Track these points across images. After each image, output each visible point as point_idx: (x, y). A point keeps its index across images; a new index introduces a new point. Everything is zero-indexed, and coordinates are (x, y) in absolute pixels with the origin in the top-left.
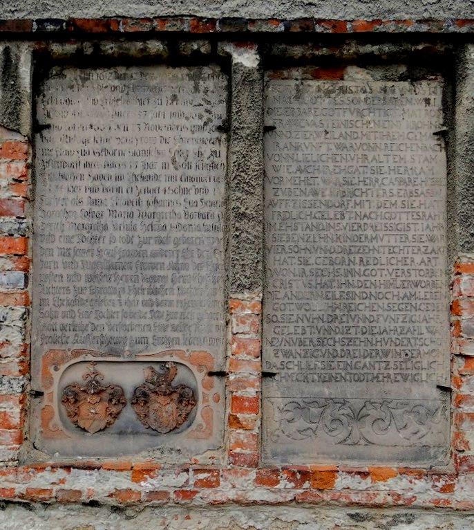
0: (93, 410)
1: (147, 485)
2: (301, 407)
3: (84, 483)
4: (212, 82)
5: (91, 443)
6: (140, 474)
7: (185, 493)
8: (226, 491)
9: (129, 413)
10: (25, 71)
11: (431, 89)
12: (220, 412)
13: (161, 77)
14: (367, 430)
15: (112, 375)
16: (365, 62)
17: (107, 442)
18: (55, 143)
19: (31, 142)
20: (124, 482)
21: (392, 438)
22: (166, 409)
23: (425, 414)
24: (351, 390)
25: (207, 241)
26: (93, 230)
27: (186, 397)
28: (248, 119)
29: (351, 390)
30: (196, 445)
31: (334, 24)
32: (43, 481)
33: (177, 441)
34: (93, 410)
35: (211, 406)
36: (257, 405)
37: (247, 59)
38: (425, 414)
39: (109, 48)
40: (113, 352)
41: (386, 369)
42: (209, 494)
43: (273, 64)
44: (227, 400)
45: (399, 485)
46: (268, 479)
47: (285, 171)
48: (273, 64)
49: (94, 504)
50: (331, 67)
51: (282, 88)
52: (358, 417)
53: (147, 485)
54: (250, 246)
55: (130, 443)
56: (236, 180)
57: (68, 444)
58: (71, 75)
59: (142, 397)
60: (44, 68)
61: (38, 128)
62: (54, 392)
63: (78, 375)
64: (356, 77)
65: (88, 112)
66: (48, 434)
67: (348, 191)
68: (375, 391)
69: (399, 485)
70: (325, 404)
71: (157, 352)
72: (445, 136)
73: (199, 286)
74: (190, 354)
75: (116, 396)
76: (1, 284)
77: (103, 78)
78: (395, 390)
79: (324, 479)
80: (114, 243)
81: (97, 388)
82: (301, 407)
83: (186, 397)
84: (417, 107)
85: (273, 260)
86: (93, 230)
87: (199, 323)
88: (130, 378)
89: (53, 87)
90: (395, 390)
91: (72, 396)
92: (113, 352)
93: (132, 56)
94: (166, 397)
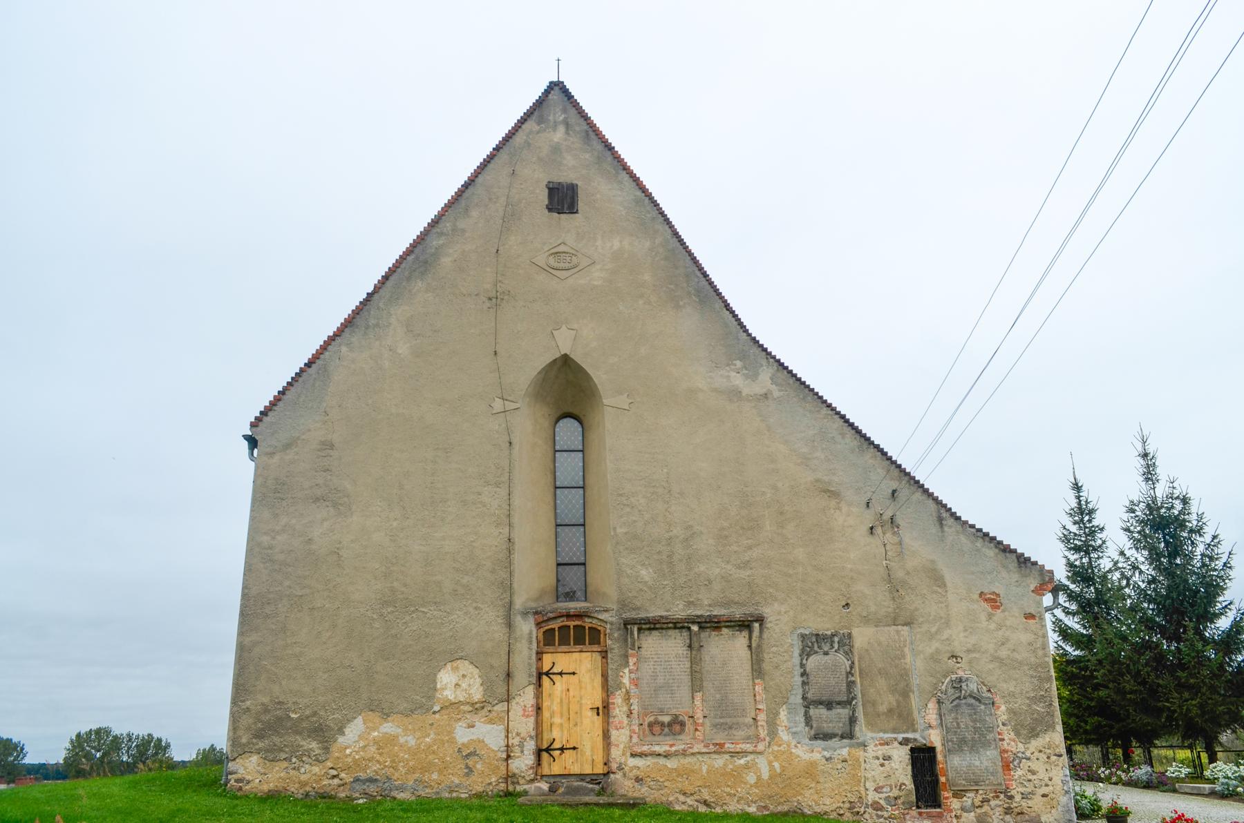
0: (657, 729)
1: (674, 749)
2: (715, 726)
3: (657, 749)
4: (685, 633)
5: (657, 738)
6: (671, 746)
9: (666, 730)
10: (636, 633)
11: (745, 633)
12: (692, 728)
13: (671, 632)
15: (661, 718)
17: (661, 738)
20: (667, 748)
21: (740, 734)
22: (677, 727)
23: (749, 726)
24: (728, 720)
25: (686, 679)
26: (654, 677)
27: (682, 724)
28: (696, 645)
29: (728, 720)
30: (685, 737)
31: (635, 798)
32: (645, 748)
33: (681, 737)
34: (657, 729)
35: (689, 726)
36: (702, 725)
38: (749, 726)
40: (662, 712)
44: (516, 447)
45: (743, 746)
46: (707, 746)
47: (706, 658)
51: (704, 635)
52: (731, 728)
53: (674, 749)
54: (696, 681)
56: (693, 662)
57: (650, 738)
59: (670, 725)
63: (652, 719)
65: (652, 644)
67: (724, 664)
68: (734, 720)
69: (743, 746)
71: (674, 711)
72: (750, 647)
73: (685, 691)
74: (682, 711)
75: (662, 724)
76: (1239, 756)
77: (655, 633)
78: (741, 720)
79: (722, 745)
80: (660, 680)
81: (656, 722)
82: (715, 726)
83: (682, 724)
84: (741, 640)
86: (654, 677)
87: (680, 701)
88: (666, 719)
90: (741, 720)
91: (651, 725)
92: (662, 712)
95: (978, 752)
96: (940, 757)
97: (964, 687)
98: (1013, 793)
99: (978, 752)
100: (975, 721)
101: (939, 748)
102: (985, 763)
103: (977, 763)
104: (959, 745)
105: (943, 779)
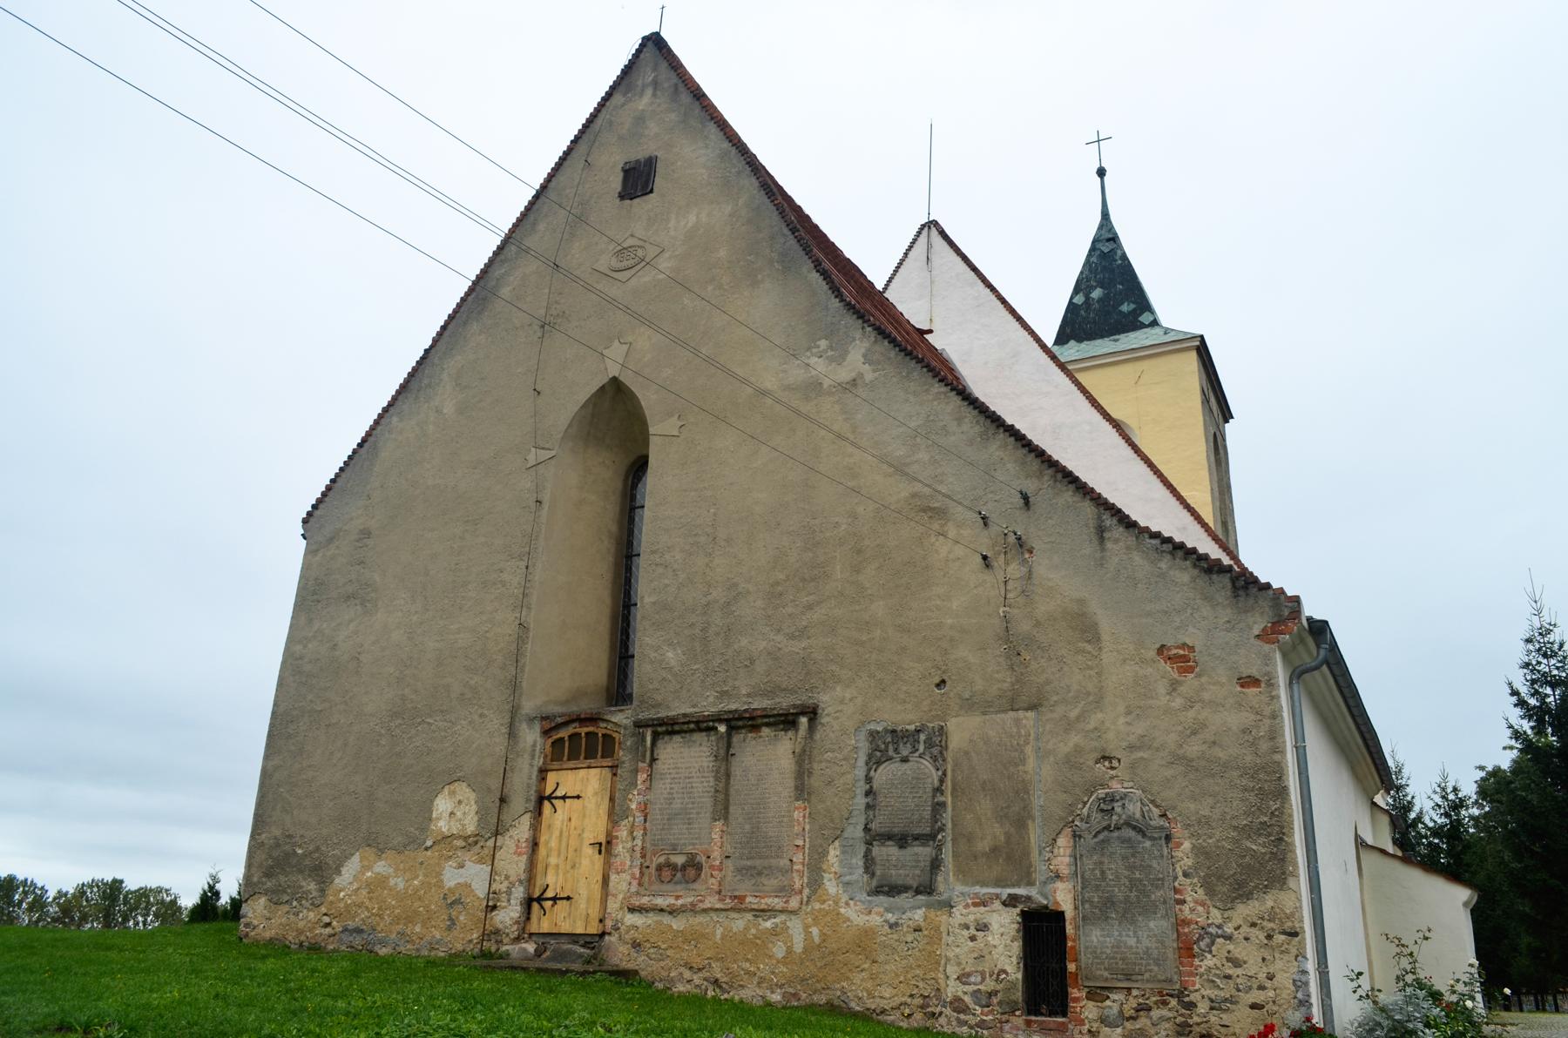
1: (680, 902)
5: (665, 887)
6: (677, 898)
7: (692, 904)
8: (707, 905)
9: (679, 875)
10: (649, 739)
13: (697, 736)
14: (764, 880)
16: (767, 725)
18: (659, 766)
19: (651, 766)
22: (691, 872)
24: (758, 862)
25: (708, 802)
29: (758, 862)
32: (645, 900)
33: (695, 886)
34: (666, 873)
37: (722, 728)
39: (677, 728)
40: (674, 849)
41: (1379, 1024)
42: (702, 906)
43: (732, 729)
48: (732, 729)
49: (662, 910)
50: (755, 728)
52: (760, 874)
53: (680, 902)
55: (678, 887)
58: (667, 738)
59: (684, 867)
60: (656, 736)
61: (653, 760)
62: (654, 866)
63: (662, 860)
64: (766, 731)
66: (651, 883)
70: (748, 868)
71: (689, 849)
75: (674, 867)
77: (677, 738)
78: (773, 862)
83: (699, 867)
85: (732, 809)
86: (670, 800)
88: (680, 860)
89: (660, 743)
90: (773, 862)
91: (659, 868)
92: (674, 849)
93: (1494, 785)
94: (692, 868)
95: (1133, 922)
96: (1069, 930)
97: (1118, 810)
98: (1194, 997)
99: (1133, 922)
100: (1132, 868)
101: (1069, 914)
102: (1146, 943)
103: (1132, 942)
104: (1101, 908)
105: (1071, 967)
